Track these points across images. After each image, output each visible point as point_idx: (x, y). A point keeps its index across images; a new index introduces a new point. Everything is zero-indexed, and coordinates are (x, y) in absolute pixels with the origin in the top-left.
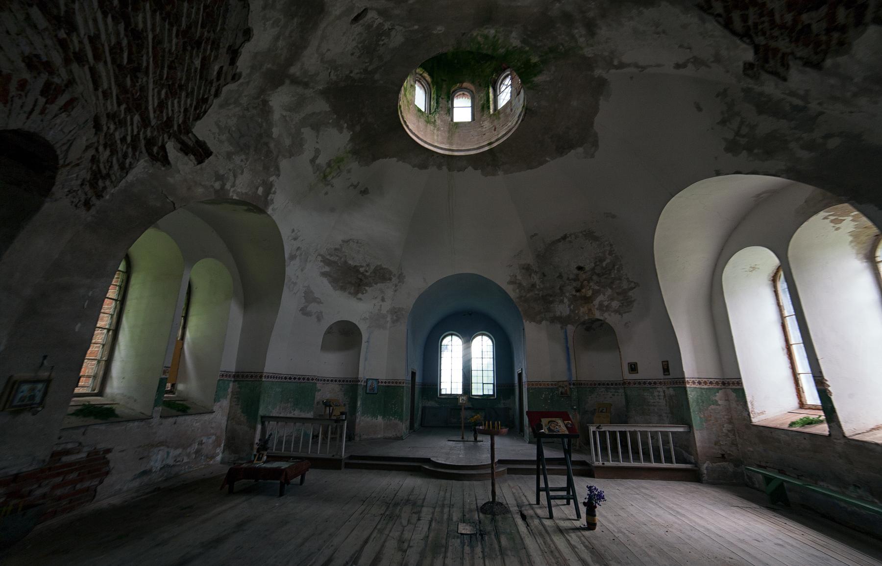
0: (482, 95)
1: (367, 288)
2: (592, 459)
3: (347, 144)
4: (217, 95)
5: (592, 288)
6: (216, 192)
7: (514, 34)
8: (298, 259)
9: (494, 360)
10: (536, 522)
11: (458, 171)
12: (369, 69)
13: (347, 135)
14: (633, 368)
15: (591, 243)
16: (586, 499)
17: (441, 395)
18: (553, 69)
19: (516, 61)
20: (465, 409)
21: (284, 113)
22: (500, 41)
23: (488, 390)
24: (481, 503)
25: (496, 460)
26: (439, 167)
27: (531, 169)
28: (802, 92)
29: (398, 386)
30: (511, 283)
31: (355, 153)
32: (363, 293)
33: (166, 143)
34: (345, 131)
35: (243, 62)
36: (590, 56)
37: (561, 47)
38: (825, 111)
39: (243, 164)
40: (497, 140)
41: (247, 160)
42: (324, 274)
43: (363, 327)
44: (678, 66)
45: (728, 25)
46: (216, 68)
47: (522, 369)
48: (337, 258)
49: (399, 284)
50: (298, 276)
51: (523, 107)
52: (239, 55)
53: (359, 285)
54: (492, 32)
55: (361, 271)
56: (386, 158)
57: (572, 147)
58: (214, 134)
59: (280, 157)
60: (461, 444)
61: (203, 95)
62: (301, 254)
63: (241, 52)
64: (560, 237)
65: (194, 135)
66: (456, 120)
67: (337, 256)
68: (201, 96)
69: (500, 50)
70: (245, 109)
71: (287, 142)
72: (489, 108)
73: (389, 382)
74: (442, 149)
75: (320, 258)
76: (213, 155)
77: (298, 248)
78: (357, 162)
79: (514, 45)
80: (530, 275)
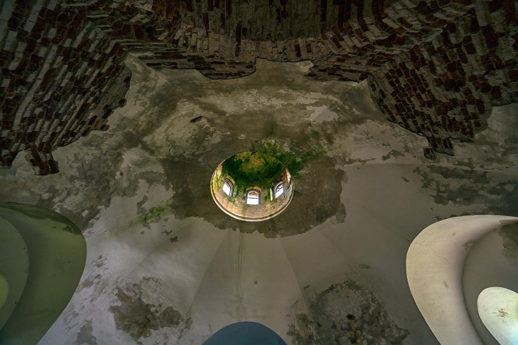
0: (266, 192)
3: (170, 200)
4: (85, 134)
5: (366, 337)
6: (42, 200)
7: (286, 144)
8: (93, 287)
11: (248, 233)
12: (196, 153)
13: (171, 193)
15: (355, 292)
18: (310, 165)
19: (287, 161)
21: (130, 165)
22: (278, 148)
26: (234, 229)
27: (300, 233)
28: (466, 161)
30: (290, 333)
31: (174, 207)
33: (21, 151)
34: (171, 189)
35: (113, 120)
36: (331, 157)
37: (314, 152)
38: (487, 170)
39: (81, 188)
41: (86, 186)
42: (113, 309)
44: (384, 158)
45: (407, 127)
46: (92, 114)
48: (133, 294)
49: (185, 330)
50: (83, 307)
51: (293, 191)
52: (111, 113)
53: (145, 326)
54: (273, 141)
55: (152, 311)
56: (196, 217)
57: (328, 216)
58: (69, 160)
59: (115, 193)
61: (73, 130)
62: (98, 283)
63: (114, 111)
64: (328, 288)
65: (52, 156)
66: (248, 203)
67: (134, 292)
68: (71, 129)
69: (278, 153)
70: (102, 154)
71: (125, 184)
72: (270, 198)
74: (237, 216)
75: (116, 291)
76: (58, 173)
77: (98, 276)
78: (174, 215)
79: (286, 151)
80: (307, 326)
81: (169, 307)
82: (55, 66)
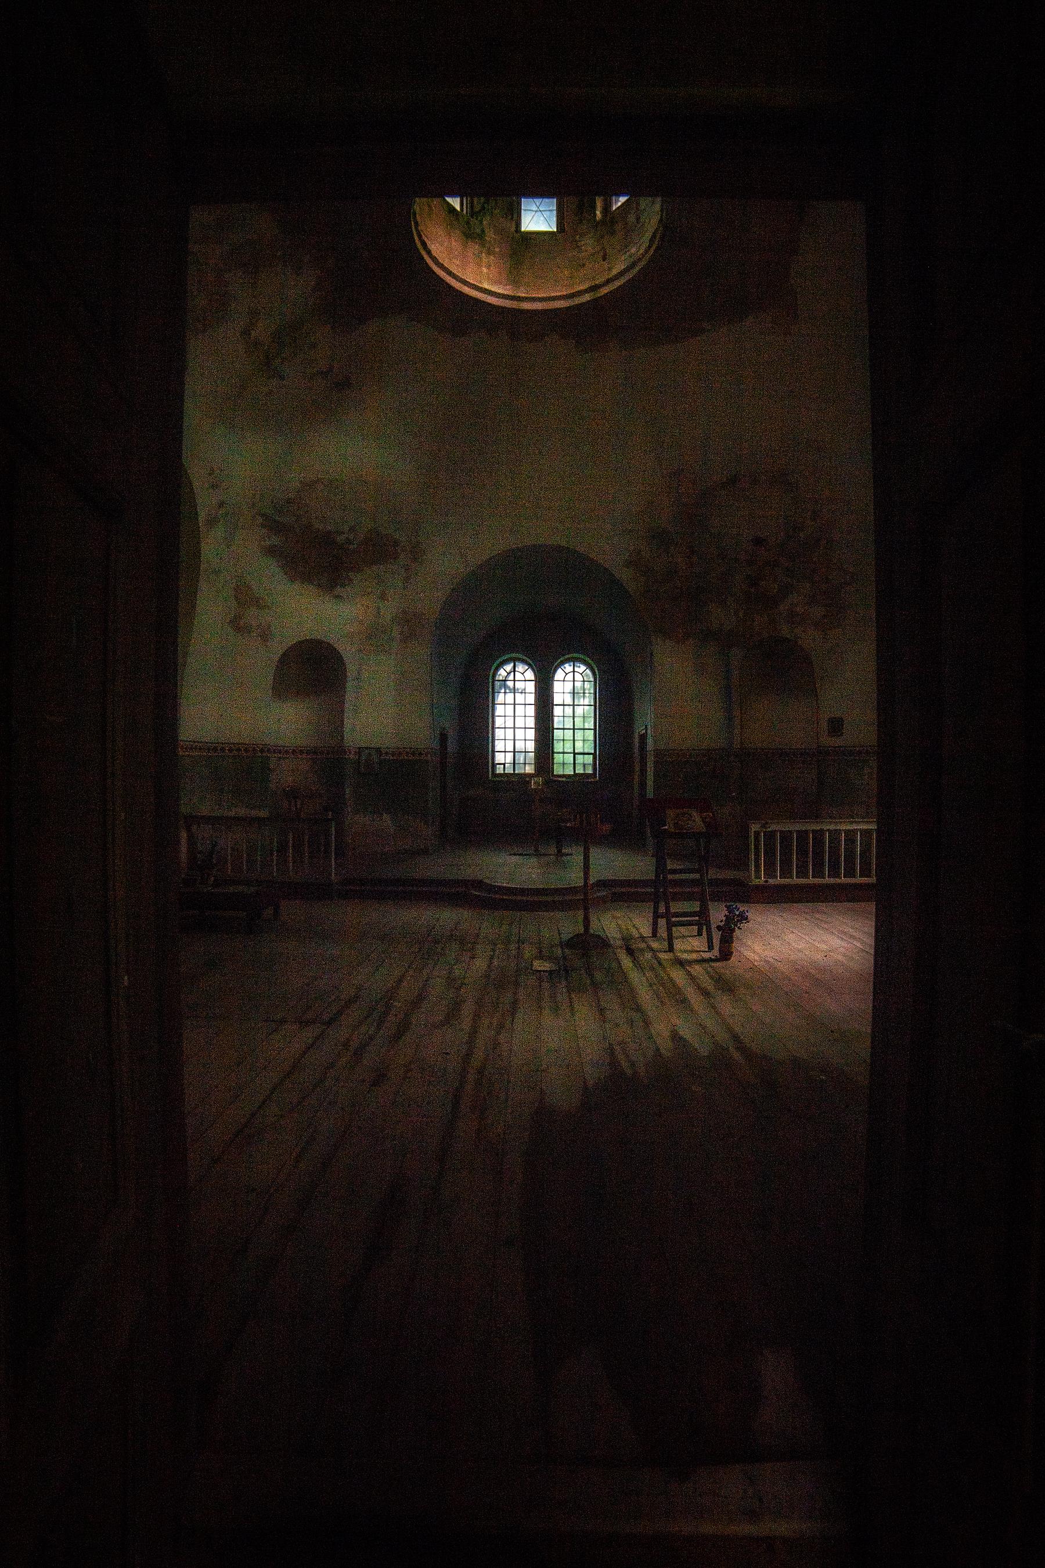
2: (749, 876)
10: (648, 955)
14: (836, 726)
16: (721, 921)
17: (495, 775)
20: (541, 800)
23: (584, 765)
24: (565, 937)
25: (592, 881)
40: (608, 281)
43: (347, 651)
47: (646, 726)
60: (534, 860)
66: (524, 228)
75: (260, 520)
77: (221, 504)
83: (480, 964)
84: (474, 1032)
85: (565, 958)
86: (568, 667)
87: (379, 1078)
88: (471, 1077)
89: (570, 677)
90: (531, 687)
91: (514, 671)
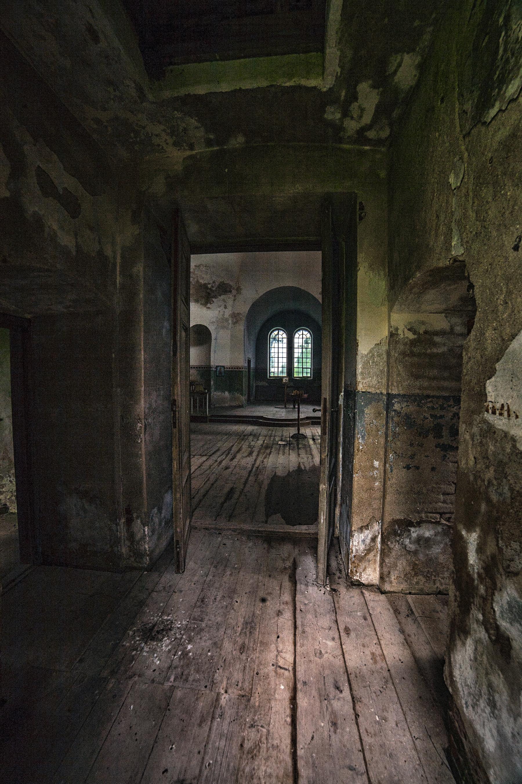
1: (213, 299)
9: (269, 356)
24: (291, 435)
29: (239, 371)
32: (211, 304)
43: (212, 328)
53: (208, 298)
60: (284, 410)
73: (232, 368)
81: (221, 282)
82: (175, 431)
83: (260, 442)
84: (255, 460)
85: (290, 441)
86: (300, 333)
87: (227, 468)
88: (254, 469)
89: (301, 336)
90: (285, 341)
91: (278, 334)
